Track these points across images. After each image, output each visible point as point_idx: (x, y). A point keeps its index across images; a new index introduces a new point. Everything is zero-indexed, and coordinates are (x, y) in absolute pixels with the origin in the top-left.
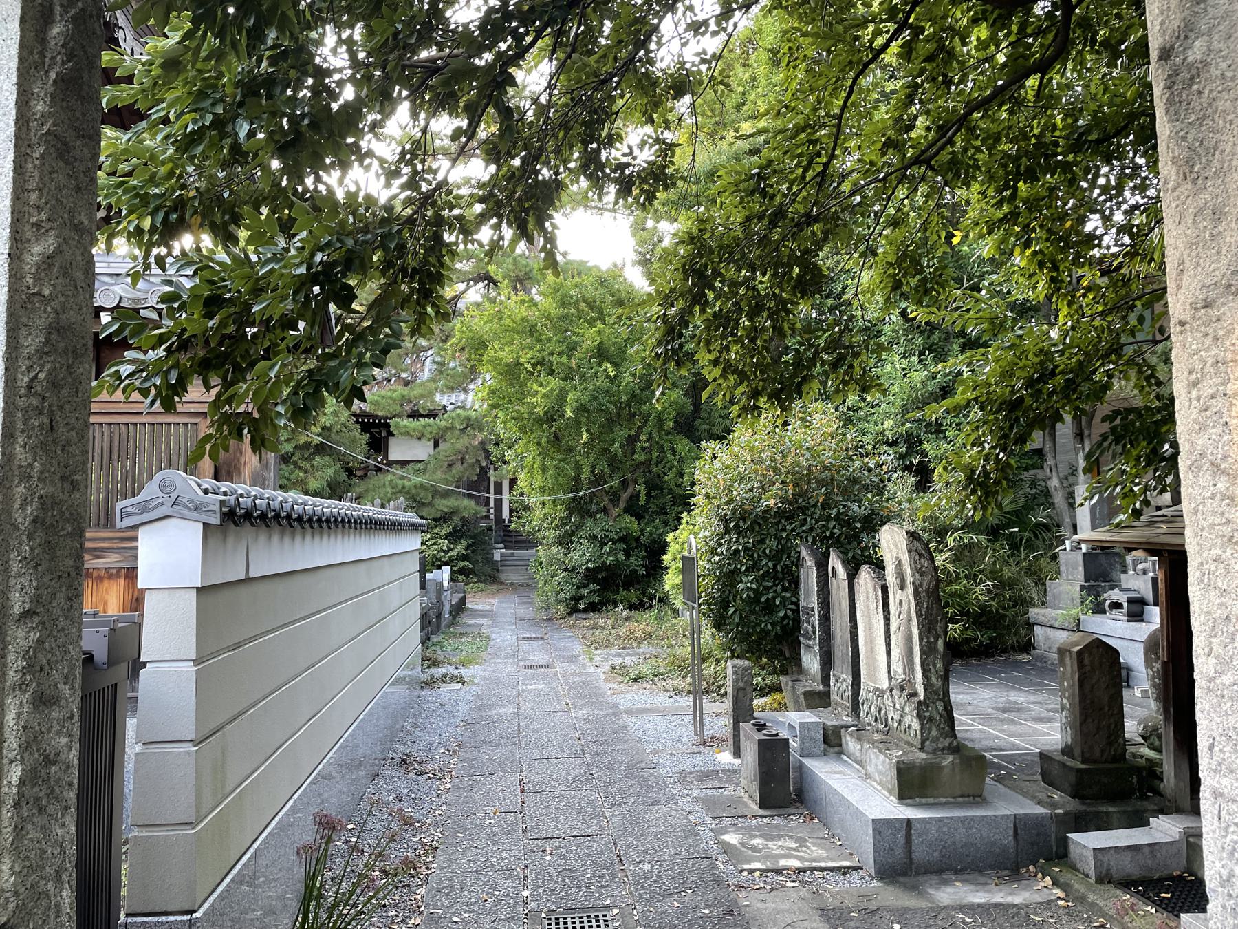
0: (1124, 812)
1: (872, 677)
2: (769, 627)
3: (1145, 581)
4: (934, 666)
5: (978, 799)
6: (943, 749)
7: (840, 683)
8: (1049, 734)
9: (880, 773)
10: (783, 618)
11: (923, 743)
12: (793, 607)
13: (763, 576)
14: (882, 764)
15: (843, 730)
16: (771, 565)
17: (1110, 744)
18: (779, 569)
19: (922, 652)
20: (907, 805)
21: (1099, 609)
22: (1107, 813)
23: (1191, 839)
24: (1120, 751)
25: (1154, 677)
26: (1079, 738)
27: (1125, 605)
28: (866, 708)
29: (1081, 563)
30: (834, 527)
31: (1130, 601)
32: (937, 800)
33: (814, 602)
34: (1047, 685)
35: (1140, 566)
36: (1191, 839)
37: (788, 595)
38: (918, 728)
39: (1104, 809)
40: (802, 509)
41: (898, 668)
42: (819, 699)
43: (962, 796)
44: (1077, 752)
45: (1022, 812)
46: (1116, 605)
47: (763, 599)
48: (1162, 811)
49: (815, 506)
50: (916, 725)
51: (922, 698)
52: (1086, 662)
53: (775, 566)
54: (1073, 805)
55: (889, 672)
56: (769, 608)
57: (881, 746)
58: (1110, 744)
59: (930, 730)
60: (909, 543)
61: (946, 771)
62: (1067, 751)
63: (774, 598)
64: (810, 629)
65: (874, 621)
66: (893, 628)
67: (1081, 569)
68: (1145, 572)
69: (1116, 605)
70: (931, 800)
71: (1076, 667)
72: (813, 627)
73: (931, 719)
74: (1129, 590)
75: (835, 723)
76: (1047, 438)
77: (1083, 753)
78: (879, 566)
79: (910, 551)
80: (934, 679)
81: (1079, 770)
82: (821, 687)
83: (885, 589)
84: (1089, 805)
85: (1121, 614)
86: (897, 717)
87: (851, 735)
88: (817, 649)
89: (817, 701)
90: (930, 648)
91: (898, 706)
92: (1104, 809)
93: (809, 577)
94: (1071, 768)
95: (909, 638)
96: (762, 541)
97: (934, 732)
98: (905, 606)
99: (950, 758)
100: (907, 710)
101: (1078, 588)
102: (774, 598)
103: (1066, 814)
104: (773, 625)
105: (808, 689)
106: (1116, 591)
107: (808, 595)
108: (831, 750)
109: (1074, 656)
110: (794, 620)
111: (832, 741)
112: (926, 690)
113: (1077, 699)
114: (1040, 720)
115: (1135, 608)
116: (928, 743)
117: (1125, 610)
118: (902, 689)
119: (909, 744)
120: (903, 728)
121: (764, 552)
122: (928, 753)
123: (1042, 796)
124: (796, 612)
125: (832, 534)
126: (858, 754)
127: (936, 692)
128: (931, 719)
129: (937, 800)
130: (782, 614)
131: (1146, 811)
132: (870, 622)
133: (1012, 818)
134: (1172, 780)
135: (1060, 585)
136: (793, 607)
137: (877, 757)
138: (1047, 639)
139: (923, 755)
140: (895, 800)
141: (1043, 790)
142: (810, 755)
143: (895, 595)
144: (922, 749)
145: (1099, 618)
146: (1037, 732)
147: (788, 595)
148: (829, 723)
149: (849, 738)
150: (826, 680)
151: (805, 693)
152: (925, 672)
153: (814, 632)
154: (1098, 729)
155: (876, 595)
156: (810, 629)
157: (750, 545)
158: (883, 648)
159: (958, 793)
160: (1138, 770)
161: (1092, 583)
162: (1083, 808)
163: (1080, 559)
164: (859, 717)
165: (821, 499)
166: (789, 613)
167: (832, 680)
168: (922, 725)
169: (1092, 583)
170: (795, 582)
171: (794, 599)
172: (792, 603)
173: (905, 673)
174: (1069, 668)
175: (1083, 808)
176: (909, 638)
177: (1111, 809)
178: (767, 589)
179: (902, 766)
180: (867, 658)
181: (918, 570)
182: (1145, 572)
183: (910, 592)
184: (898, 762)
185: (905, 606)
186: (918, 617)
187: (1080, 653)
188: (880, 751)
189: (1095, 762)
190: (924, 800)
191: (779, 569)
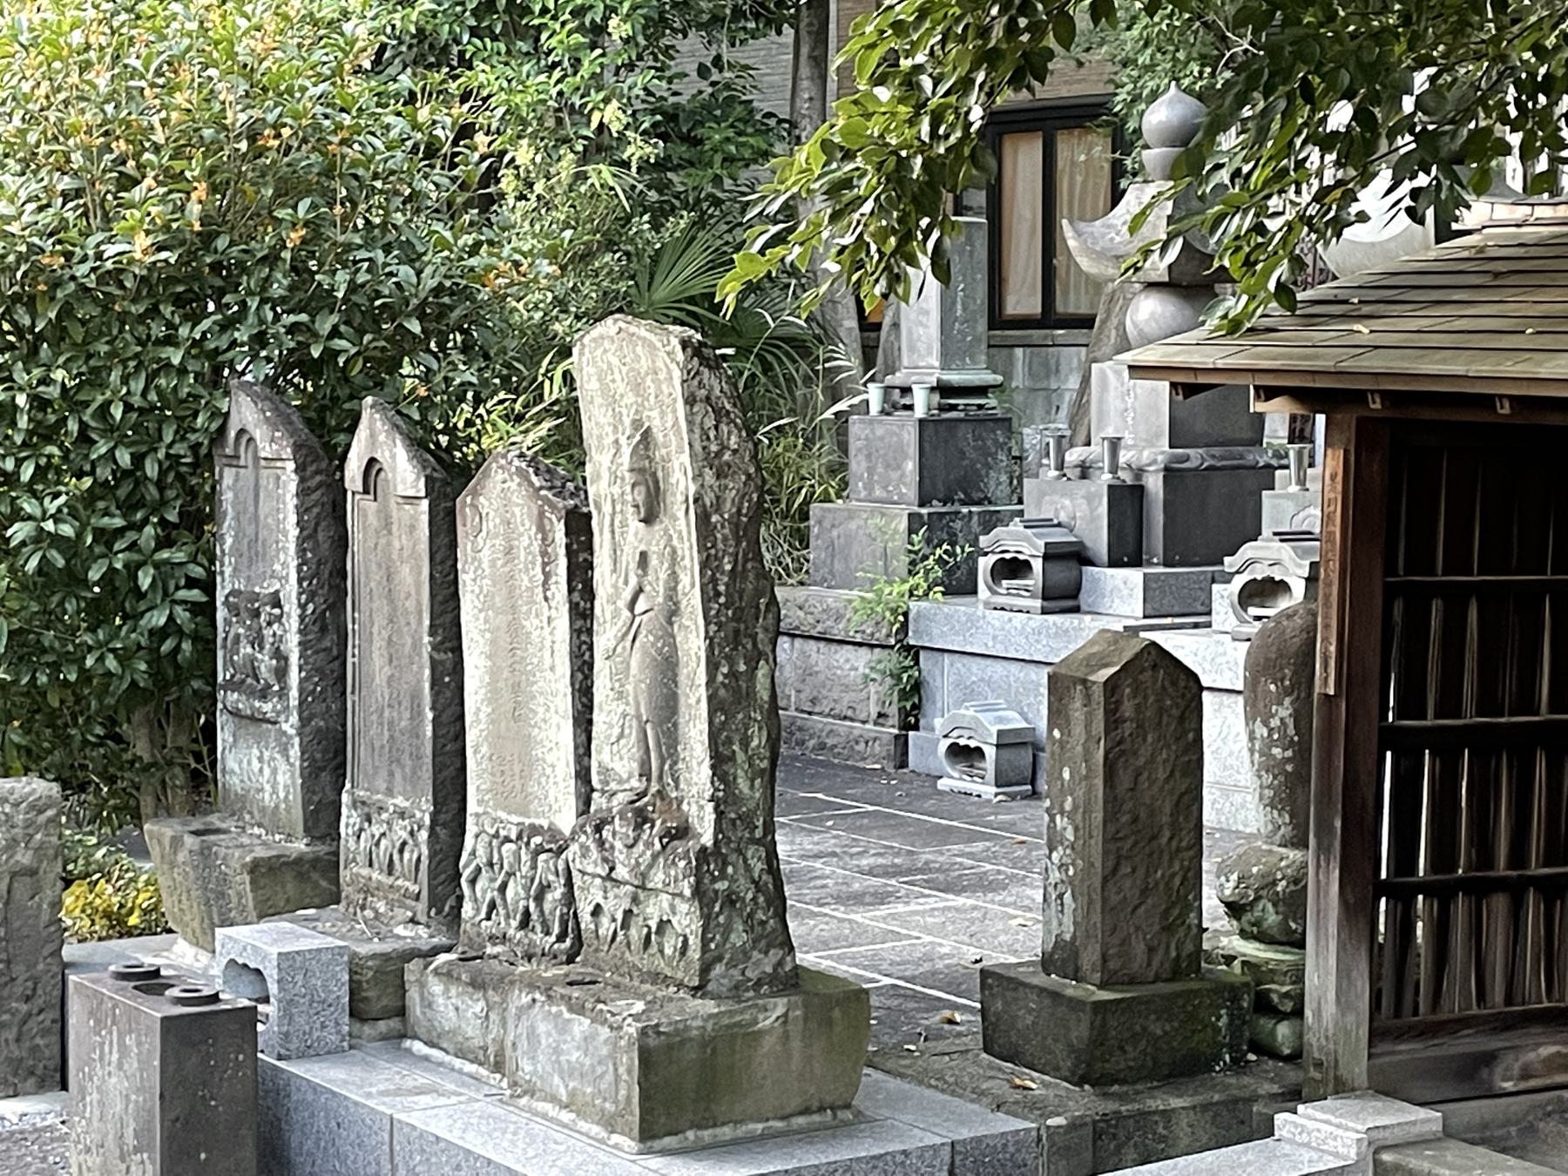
0: (1205, 1107)
1: (512, 794)
2: (111, 663)
3: (1090, 498)
4: (745, 744)
5: (847, 1115)
6: (759, 984)
7: (385, 822)
8: (898, 936)
9: (568, 1072)
10: (159, 634)
11: (705, 970)
12: (195, 595)
13: (90, 498)
14: (580, 1047)
15: (412, 969)
16: (124, 458)
17: (1168, 929)
18: (151, 469)
19: (715, 705)
20: (664, 1152)
21: (960, 584)
22: (1167, 1114)
23: (1386, 1157)
24: (1189, 947)
25: (1269, 743)
26: (1097, 918)
27: (1037, 565)
28: (486, 888)
29: (913, 450)
30: (335, 333)
31: (1052, 555)
32: (742, 1130)
33: (285, 574)
34: (829, 805)
35: (1073, 456)
36: (1386, 1157)
37: (180, 556)
38: (697, 925)
39: (1156, 1103)
40: (227, 275)
41: (617, 759)
42: (308, 880)
43: (806, 1111)
44: (1089, 958)
45: (965, 1134)
46: (1013, 568)
47: (94, 575)
48: (1294, 1097)
49: (272, 259)
50: (687, 920)
51: (707, 839)
52: (1127, 709)
53: (138, 460)
54: (1083, 1103)
55: (583, 775)
56: (118, 598)
57: (576, 992)
58: (1168, 929)
59: (727, 930)
60: (689, 377)
61: (768, 1043)
62: (1059, 959)
63: (132, 569)
64: (266, 663)
65: (530, 624)
66: (604, 640)
67: (911, 466)
68: (1085, 471)
69: (1013, 568)
70: (726, 1132)
71: (1099, 726)
72: (280, 656)
73: (731, 900)
74: (1046, 523)
75: (377, 947)
76: (805, 71)
77: (1105, 959)
78: (567, 443)
79: (690, 401)
80: (743, 784)
81: (1099, 1006)
82: (300, 846)
83: (579, 526)
84: (1122, 1098)
85: (1025, 593)
86: (615, 905)
87: (447, 975)
88: (290, 725)
89: (291, 888)
90: (736, 691)
91: (621, 872)
92: (1156, 1103)
93: (263, 495)
94: (1075, 1004)
95: (667, 667)
96: (95, 379)
97: (739, 938)
98: (659, 571)
99: (780, 1006)
100: (657, 878)
101: (903, 525)
102: (132, 569)
103: (1073, 1126)
104: (124, 658)
105: (261, 852)
106: (1016, 526)
107: (255, 552)
108: (367, 1029)
109: (1098, 694)
110: (196, 638)
111: (377, 1004)
112: (720, 814)
113: (1098, 816)
114: (857, 899)
115: (1063, 573)
116: (718, 969)
117: (1035, 580)
118: (641, 819)
119: (656, 977)
120: (635, 934)
121: (104, 411)
122: (716, 997)
123: (998, 1087)
124: (205, 611)
125: (331, 354)
126: (472, 1030)
127: (747, 820)
128: (731, 900)
129: (742, 1130)
130: (159, 619)
131: (1254, 1098)
132: (514, 629)
133: (946, 1154)
134: (1330, 1009)
135: (852, 515)
136: (195, 595)
137: (563, 1028)
138: (807, 673)
139: (710, 1006)
140: (629, 1144)
141: (1001, 1076)
142: (308, 1052)
143: (619, 539)
144: (699, 990)
145: (960, 607)
146: (860, 934)
147: (180, 556)
148: (363, 949)
149: (436, 987)
150: (322, 818)
151: (255, 868)
152: (720, 761)
153: (281, 673)
154: (1145, 892)
155: (546, 541)
156: (266, 663)
157: (53, 392)
158: (564, 703)
159: (795, 1103)
160: (1232, 992)
161: (937, 507)
162: (1111, 1106)
163: (911, 436)
164: (454, 918)
165: (294, 237)
166: (182, 615)
167: (349, 819)
168: (707, 918)
169: (937, 507)
170: (197, 520)
171: (197, 571)
172: (191, 583)
173: (645, 773)
174: (1078, 730)
175: (1111, 1106)
176: (667, 667)
177: (1176, 1103)
178: (106, 538)
179: (652, 1041)
180: (495, 738)
181: (710, 461)
182: (1085, 471)
183: (681, 525)
184: (643, 1032)
185: (659, 571)
186: (706, 601)
187: (1111, 685)
188: (579, 1009)
189: (1132, 982)
190: (707, 1134)
191: (151, 469)
